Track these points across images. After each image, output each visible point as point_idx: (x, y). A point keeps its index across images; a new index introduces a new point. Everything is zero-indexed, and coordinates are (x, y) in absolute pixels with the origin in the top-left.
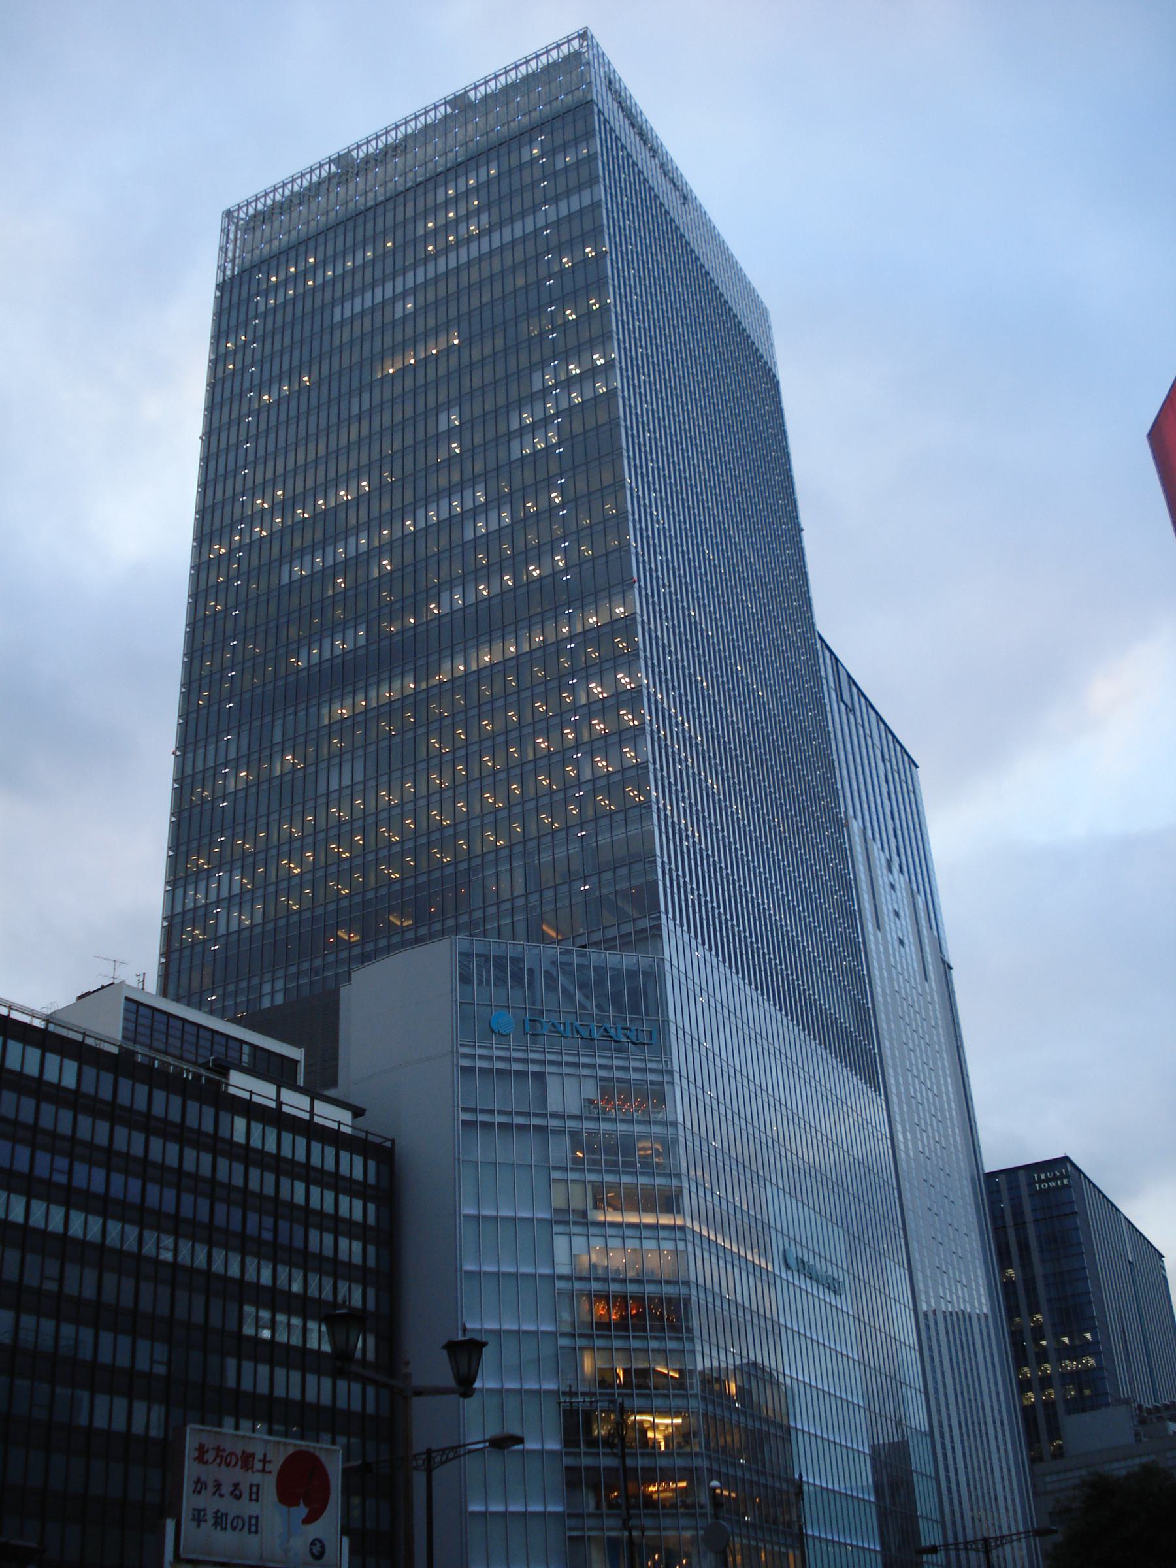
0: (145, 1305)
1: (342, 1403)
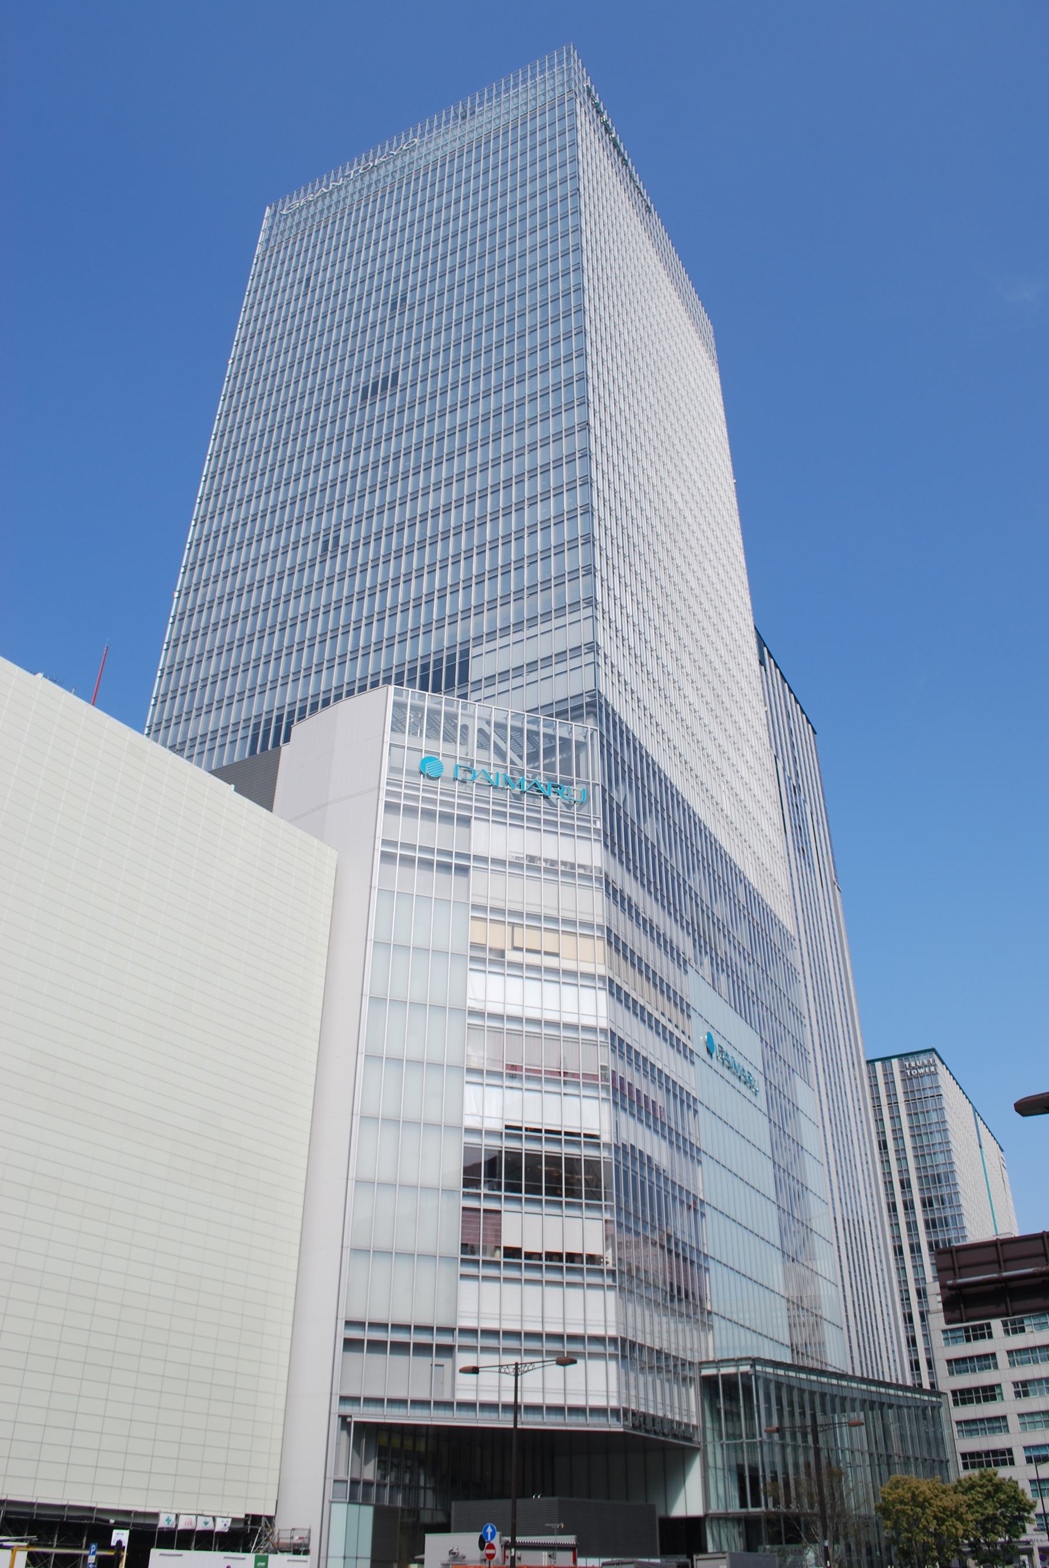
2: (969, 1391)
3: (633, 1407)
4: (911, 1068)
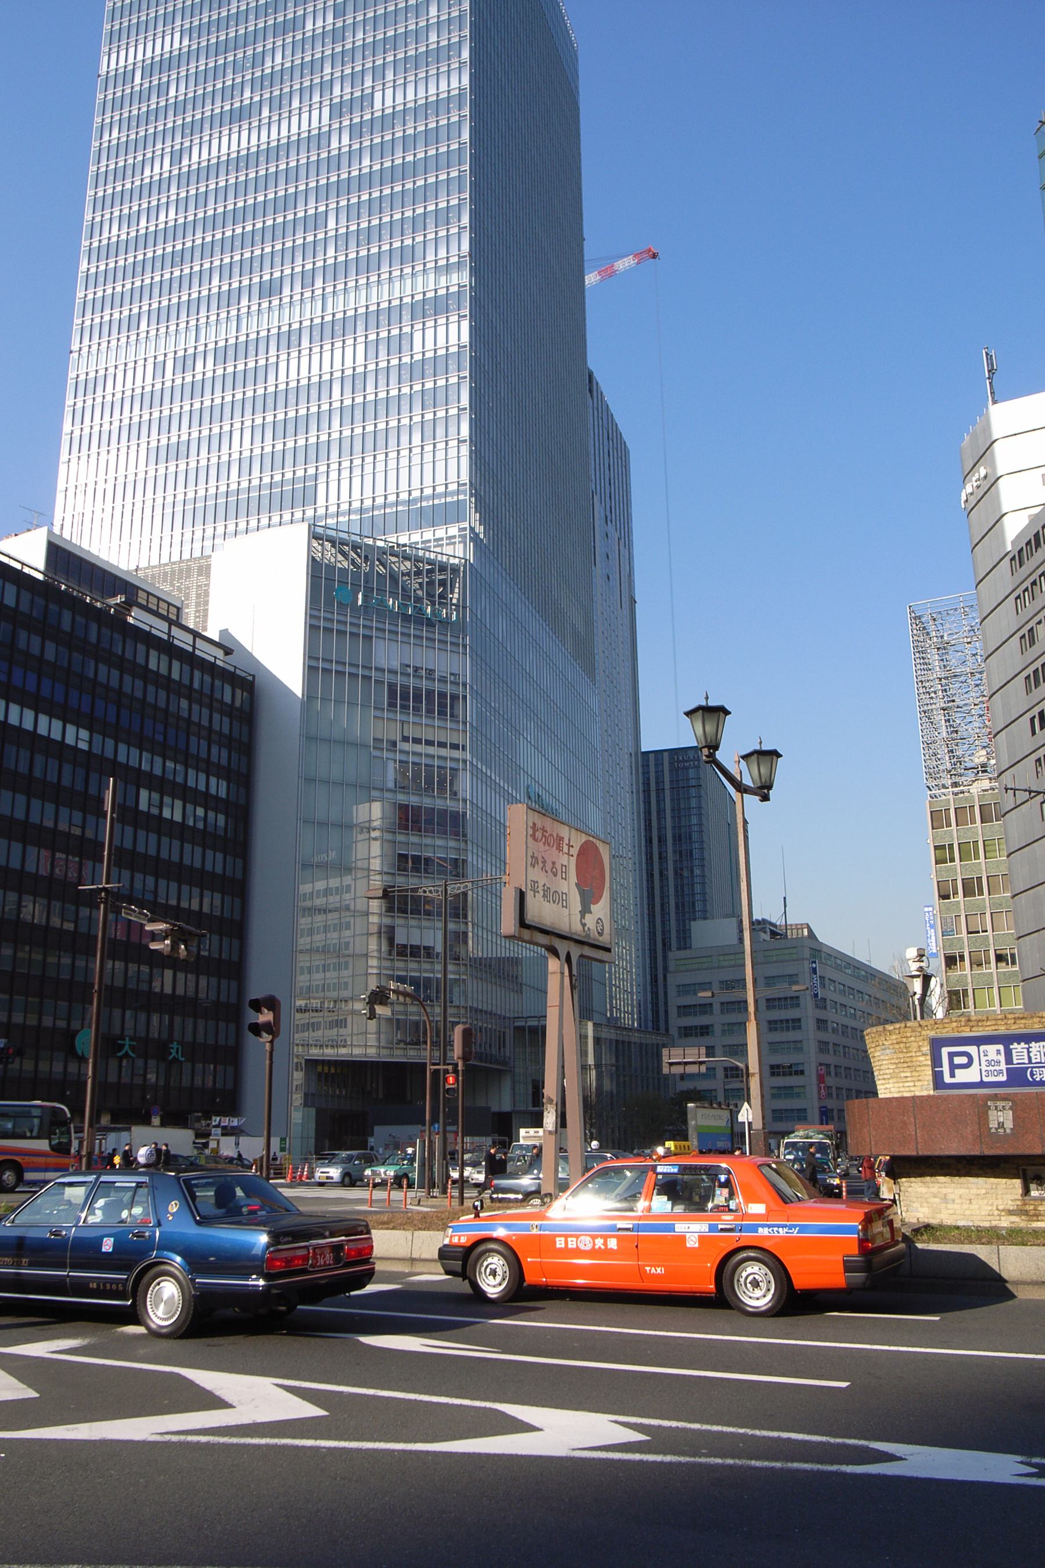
0: (66, 782)
1: (209, 867)
2: (691, 1028)
3: (475, 1005)
4: (678, 761)
